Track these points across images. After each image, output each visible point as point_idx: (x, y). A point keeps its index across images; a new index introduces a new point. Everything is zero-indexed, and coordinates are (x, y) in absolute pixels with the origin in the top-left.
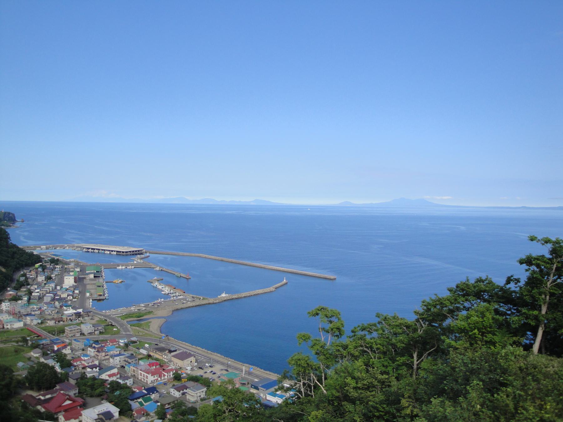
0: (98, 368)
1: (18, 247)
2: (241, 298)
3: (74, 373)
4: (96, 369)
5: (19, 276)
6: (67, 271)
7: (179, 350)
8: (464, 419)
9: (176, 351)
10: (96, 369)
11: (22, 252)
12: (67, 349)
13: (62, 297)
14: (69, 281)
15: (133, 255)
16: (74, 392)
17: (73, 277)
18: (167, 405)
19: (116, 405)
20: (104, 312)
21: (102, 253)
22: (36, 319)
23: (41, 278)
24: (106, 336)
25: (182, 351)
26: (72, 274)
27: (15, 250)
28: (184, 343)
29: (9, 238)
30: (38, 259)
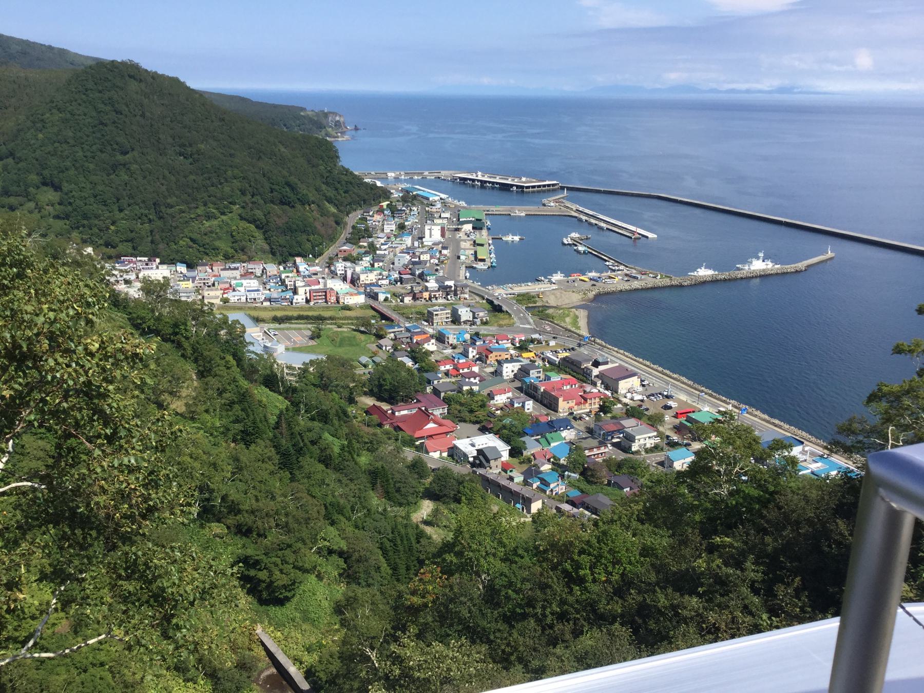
0: (478, 378)
1: (352, 173)
2: (736, 279)
3: (441, 381)
4: (475, 379)
5: (749, 260)
6: (429, 217)
7: (613, 362)
8: (213, 675)
9: (606, 363)
10: (475, 379)
11: (357, 182)
12: (430, 343)
13: (421, 259)
14: (433, 234)
15: (544, 191)
16: (441, 411)
17: (439, 227)
18: (595, 450)
19: (507, 440)
20: (490, 287)
21: (526, 192)
22: (383, 293)
23: (390, 227)
24: (491, 328)
25: (617, 364)
26: (437, 221)
27: (350, 178)
28: (622, 351)
29: (338, 157)
30: (385, 194)
